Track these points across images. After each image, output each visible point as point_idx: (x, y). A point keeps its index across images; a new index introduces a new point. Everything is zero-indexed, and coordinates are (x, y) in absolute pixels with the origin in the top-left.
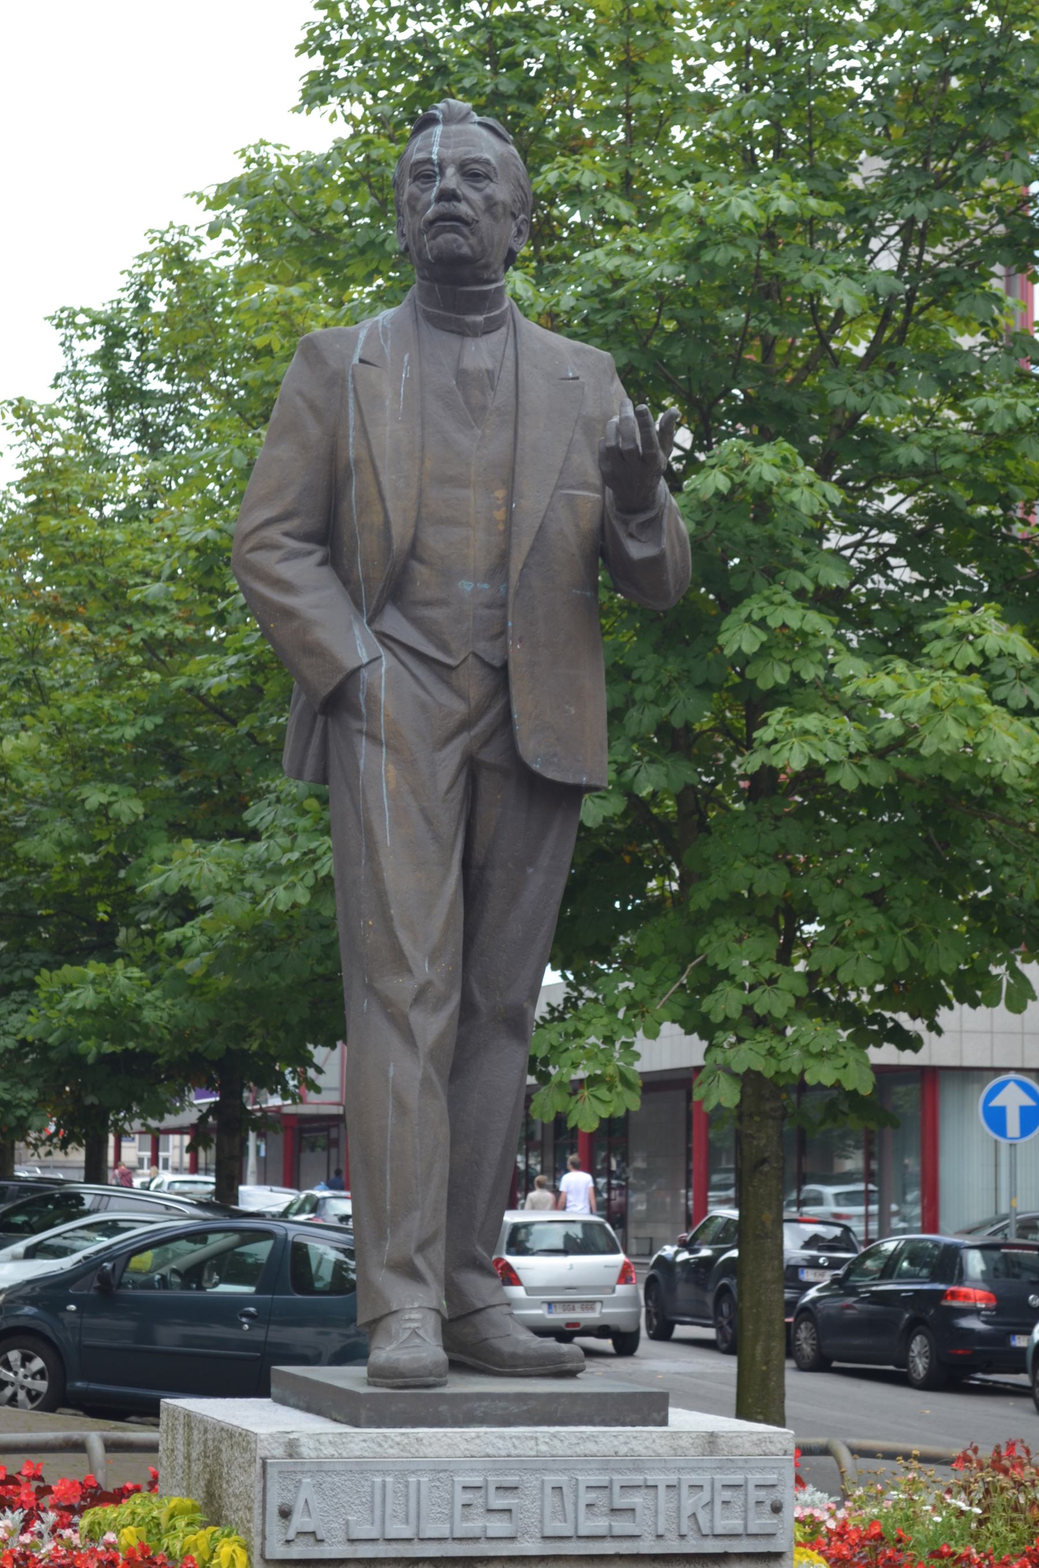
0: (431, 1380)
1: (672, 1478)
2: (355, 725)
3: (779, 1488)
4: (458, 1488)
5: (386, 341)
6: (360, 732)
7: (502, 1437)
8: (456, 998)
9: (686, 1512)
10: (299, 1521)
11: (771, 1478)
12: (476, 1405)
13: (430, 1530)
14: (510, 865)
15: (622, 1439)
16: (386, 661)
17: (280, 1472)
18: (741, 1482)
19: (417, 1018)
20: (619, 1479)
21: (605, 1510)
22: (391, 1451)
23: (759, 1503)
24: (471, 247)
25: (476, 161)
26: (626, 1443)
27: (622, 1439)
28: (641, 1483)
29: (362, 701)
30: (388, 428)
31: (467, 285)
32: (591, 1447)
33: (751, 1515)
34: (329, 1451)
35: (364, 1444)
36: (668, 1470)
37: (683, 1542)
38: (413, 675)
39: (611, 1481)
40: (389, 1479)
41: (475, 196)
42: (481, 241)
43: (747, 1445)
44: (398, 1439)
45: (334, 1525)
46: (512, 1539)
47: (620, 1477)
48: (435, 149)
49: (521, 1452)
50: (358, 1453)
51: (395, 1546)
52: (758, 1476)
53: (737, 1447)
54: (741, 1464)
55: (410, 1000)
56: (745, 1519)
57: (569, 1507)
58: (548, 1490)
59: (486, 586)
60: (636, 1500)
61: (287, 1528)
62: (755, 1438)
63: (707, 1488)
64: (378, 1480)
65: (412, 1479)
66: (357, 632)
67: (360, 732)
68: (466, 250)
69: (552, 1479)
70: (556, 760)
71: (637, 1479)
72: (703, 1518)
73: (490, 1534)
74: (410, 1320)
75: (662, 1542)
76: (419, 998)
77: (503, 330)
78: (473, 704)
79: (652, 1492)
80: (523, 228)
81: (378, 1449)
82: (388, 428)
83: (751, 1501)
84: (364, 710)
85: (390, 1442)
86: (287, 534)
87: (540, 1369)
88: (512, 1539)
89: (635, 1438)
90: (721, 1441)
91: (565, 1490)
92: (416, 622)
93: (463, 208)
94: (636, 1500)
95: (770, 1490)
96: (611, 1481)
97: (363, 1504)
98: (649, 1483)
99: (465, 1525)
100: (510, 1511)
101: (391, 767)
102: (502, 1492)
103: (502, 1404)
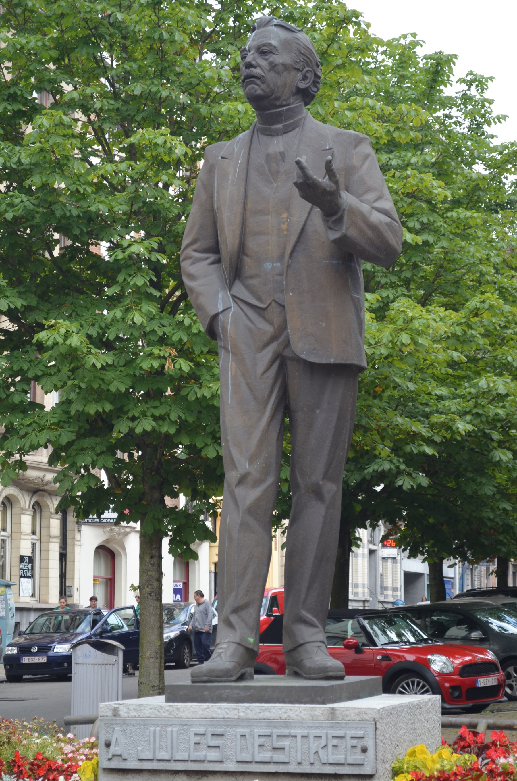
1: (305, 732)
3: (366, 739)
4: (192, 735)
7: (220, 708)
10: (113, 749)
11: (360, 733)
12: (223, 692)
14: (305, 409)
15: (283, 710)
16: (234, 308)
17: (105, 724)
18: (343, 735)
20: (276, 731)
21: (270, 748)
22: (164, 714)
23: (353, 747)
24: (263, 90)
25: (264, 45)
26: (286, 713)
27: (283, 710)
28: (288, 734)
30: (229, 190)
31: (269, 110)
32: (267, 715)
33: (349, 753)
34: (133, 714)
35: (151, 711)
36: (304, 727)
37: (313, 767)
39: (345, 734)
40: (158, 729)
41: (264, 63)
42: (268, 86)
43: (353, 715)
44: (167, 708)
45: (132, 752)
46: (221, 762)
47: (277, 730)
49: (231, 716)
50: (148, 715)
51: (162, 763)
52: (353, 732)
53: (347, 716)
54: (344, 725)
55: (235, 483)
56: (346, 755)
57: (250, 746)
58: (239, 737)
59: (279, 264)
60: (286, 743)
61: (108, 752)
62: (356, 711)
63: (324, 738)
64: (152, 729)
65: (169, 729)
66: (220, 296)
67: (221, 346)
68: (259, 92)
69: (241, 731)
70: (315, 351)
71: (286, 732)
72: (321, 753)
73: (209, 759)
74: (221, 648)
75: (301, 767)
78: (276, 326)
79: (294, 739)
81: (158, 713)
82: (229, 190)
83: (349, 747)
85: (163, 710)
86: (195, 251)
87: (319, 676)
88: (221, 762)
89: (291, 710)
90: (337, 712)
91: (247, 736)
92: (247, 287)
93: (257, 71)
94: (286, 743)
95: (360, 740)
96: (345, 734)
97: (146, 741)
98: (293, 734)
99: (196, 754)
100: (218, 747)
101: (233, 363)
102: (215, 737)
103: (237, 691)
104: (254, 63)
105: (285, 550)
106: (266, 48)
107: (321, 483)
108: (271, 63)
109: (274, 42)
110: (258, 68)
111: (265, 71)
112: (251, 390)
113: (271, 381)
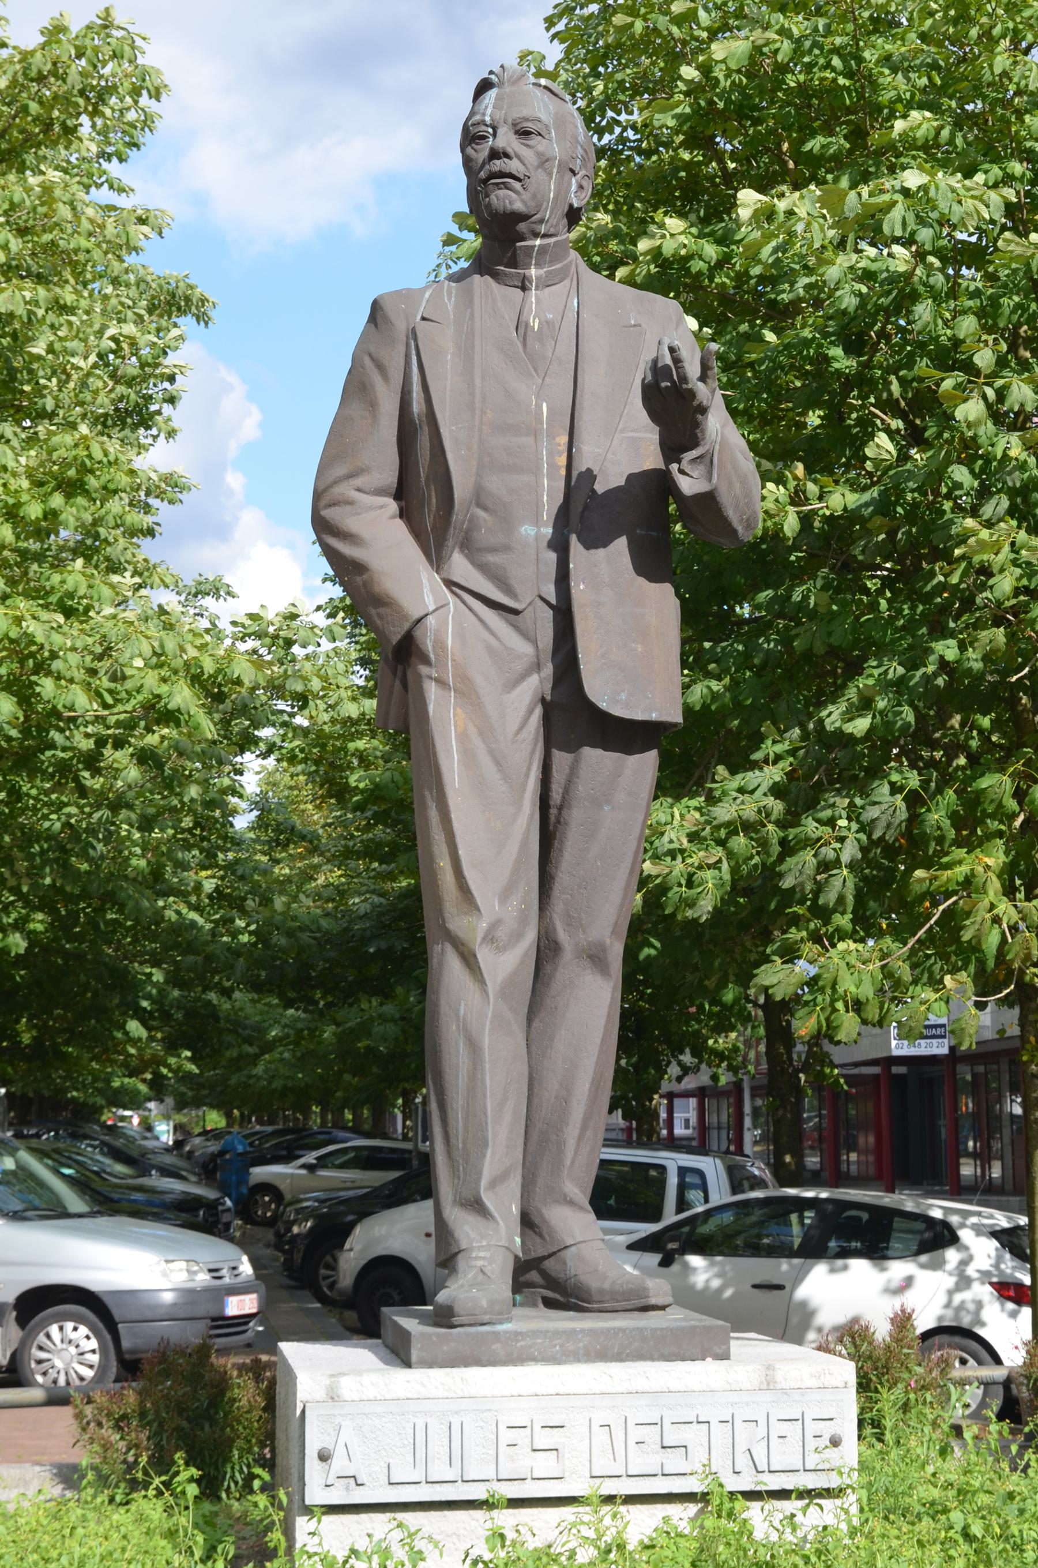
0: (486, 1318)
2: (424, 670)
5: (450, 299)
6: (430, 678)
8: (531, 936)
9: (741, 1447)
10: (339, 1464)
13: (440, 1470)
18: (658, 1420)
19: (484, 956)
24: (523, 202)
25: (527, 120)
29: (430, 648)
38: (481, 620)
48: (489, 111)
60: (692, 1435)
63: (762, 1423)
67: (430, 678)
74: (477, 1258)
76: (490, 938)
77: (567, 282)
80: (584, 183)
84: (432, 656)
87: (624, 1304)
92: (484, 568)
93: (513, 166)
104: (509, 150)
106: (530, 126)
107: (608, 941)
108: (539, 154)
109: (543, 117)
110: (515, 159)
112: (497, 763)
113: (529, 748)
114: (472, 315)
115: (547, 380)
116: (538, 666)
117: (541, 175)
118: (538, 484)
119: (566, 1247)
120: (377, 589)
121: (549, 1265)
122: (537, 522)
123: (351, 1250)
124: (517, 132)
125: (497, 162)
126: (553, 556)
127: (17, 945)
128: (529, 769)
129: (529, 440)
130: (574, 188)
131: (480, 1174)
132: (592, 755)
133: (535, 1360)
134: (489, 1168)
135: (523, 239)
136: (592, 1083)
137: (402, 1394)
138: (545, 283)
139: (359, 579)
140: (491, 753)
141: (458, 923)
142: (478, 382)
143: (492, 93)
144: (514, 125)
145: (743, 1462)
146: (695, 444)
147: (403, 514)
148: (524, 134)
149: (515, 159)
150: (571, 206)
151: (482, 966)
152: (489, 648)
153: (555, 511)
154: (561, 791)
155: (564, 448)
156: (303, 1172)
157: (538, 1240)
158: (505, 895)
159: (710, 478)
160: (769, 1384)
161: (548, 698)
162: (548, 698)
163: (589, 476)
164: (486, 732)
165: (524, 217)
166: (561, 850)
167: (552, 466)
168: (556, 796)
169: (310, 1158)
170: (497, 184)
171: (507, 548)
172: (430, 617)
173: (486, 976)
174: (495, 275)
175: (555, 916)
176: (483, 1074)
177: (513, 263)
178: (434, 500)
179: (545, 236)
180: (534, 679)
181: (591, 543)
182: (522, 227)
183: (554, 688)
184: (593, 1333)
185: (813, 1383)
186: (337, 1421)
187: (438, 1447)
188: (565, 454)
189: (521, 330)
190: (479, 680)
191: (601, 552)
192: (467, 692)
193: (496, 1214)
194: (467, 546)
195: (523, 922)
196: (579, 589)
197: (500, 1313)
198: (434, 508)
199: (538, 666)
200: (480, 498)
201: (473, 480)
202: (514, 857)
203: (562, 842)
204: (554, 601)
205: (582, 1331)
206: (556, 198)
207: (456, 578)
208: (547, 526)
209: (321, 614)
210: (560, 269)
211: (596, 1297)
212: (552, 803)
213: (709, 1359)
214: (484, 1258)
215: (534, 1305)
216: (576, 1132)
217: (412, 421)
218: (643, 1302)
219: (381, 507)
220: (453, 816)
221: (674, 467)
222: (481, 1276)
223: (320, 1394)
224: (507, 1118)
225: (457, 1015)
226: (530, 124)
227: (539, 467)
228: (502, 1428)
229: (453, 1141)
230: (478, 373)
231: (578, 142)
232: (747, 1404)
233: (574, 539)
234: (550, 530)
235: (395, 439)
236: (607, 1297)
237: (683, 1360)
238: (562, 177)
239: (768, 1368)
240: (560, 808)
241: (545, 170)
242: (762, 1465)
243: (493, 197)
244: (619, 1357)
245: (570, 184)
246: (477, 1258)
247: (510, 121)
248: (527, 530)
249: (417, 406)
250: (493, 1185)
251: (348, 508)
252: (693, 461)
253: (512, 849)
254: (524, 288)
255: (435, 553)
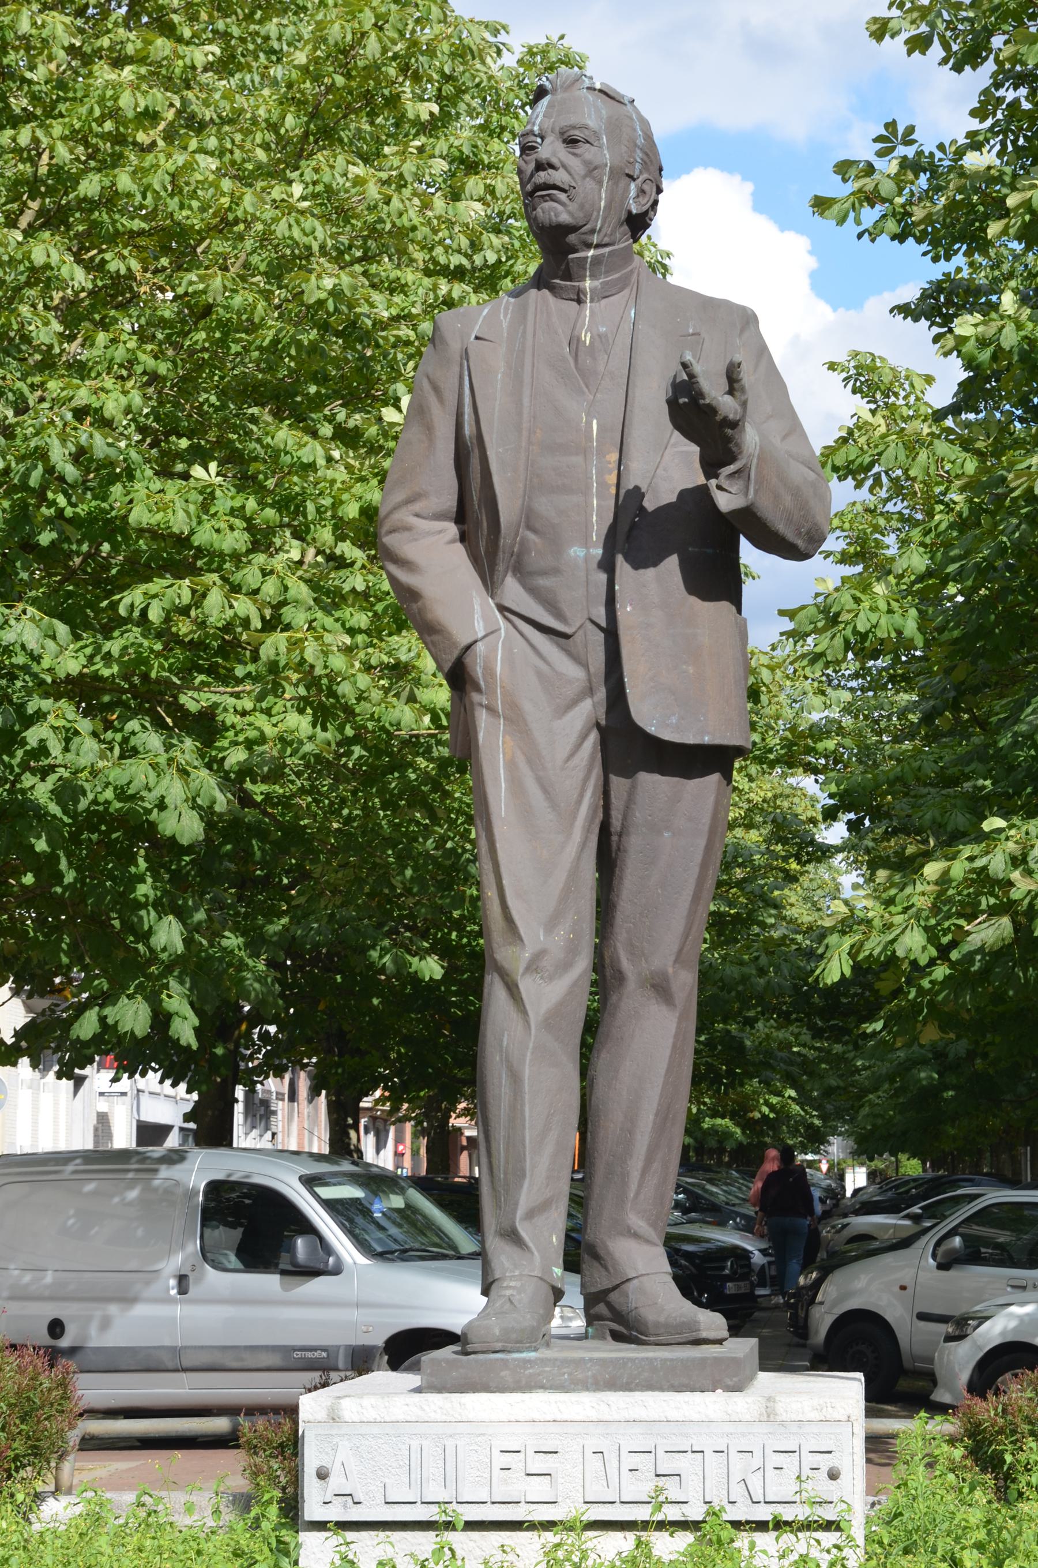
0: (498, 1346)
2: (476, 697)
4: (496, 1452)
6: (481, 705)
8: (583, 963)
10: (336, 1483)
19: (526, 986)
24: (569, 213)
25: (574, 128)
29: (480, 675)
64: (415, 1444)
67: (481, 705)
69: (593, 1443)
72: (755, 1483)
74: (508, 1287)
76: (532, 967)
80: (646, 187)
84: (482, 683)
87: (678, 1338)
92: (534, 592)
93: (558, 177)
101: (508, 738)
104: (554, 161)
105: (322, 1099)
106: (577, 134)
107: (670, 970)
108: (586, 163)
109: (592, 123)
110: (561, 170)
111: (577, 177)
112: (545, 790)
113: (581, 775)
114: (524, 332)
115: (598, 395)
116: (591, 691)
117: (590, 184)
118: (588, 505)
119: (628, 1280)
120: (429, 616)
121: (613, 1297)
122: (586, 543)
123: (822, 1303)
124: (565, 141)
125: (542, 174)
126: (603, 577)
127: (431, 970)
128: (581, 796)
129: (578, 460)
130: (633, 193)
131: (516, 1204)
132: (647, 779)
133: (543, 1387)
134: (526, 1198)
135: (576, 251)
136: (657, 1115)
137: (401, 1417)
138: (601, 295)
139: (414, 606)
140: (540, 781)
141: (504, 953)
142: (526, 401)
143: (545, 101)
144: (562, 133)
145: (738, 1492)
146: (732, 458)
147: (463, 538)
148: (571, 142)
149: (561, 170)
150: (630, 212)
151: (524, 996)
152: (539, 674)
153: (605, 531)
154: (620, 817)
155: (614, 465)
156: (907, 1222)
157: (604, 1273)
158: (551, 925)
159: (746, 494)
160: (769, 1416)
161: (603, 722)
162: (603, 722)
163: (637, 494)
164: (534, 759)
165: (573, 229)
166: (621, 878)
167: (602, 484)
168: (616, 824)
169: (916, 1210)
170: (542, 196)
171: (556, 571)
172: (479, 644)
173: (528, 1007)
174: (552, 289)
175: (618, 945)
176: (523, 1105)
177: (568, 276)
178: (485, 524)
179: (598, 246)
180: (587, 705)
181: (638, 563)
182: (572, 238)
183: (608, 712)
184: (602, 1362)
185: (815, 1416)
186: (335, 1441)
187: (433, 1469)
188: (616, 472)
189: (574, 346)
190: (527, 707)
191: (650, 573)
192: (516, 721)
193: (531, 1245)
194: (520, 570)
195: (572, 950)
196: (625, 611)
197: (521, 1342)
198: (485, 532)
199: (591, 691)
200: (529, 519)
201: (520, 502)
202: (561, 885)
203: (622, 870)
204: (604, 624)
205: (591, 1360)
206: (608, 207)
207: (508, 604)
208: (595, 547)
209: (272, 652)
210: (618, 279)
211: (652, 1331)
212: (612, 830)
213: (719, 1391)
214: (513, 1288)
215: (604, 1338)
216: (640, 1164)
217: (465, 443)
218: (694, 1335)
219: (440, 532)
220: (498, 845)
221: (713, 482)
222: (508, 1306)
223: (322, 1415)
224: (549, 1148)
225: (501, 1046)
226: (577, 132)
227: (589, 487)
228: (496, 1452)
229: (495, 1171)
230: (526, 392)
231: (636, 145)
232: (743, 1434)
233: (620, 559)
234: (600, 551)
235: (452, 462)
236: (662, 1331)
237: (693, 1391)
238: (616, 184)
239: (769, 1399)
240: (620, 835)
241: (594, 178)
242: (758, 1496)
243: (539, 210)
244: (628, 1387)
245: (627, 190)
246: (508, 1287)
247: (557, 129)
248: (576, 552)
249: (468, 430)
250: (530, 1215)
251: (406, 534)
252: (731, 476)
253: (560, 877)
254: (579, 301)
255: (489, 580)
